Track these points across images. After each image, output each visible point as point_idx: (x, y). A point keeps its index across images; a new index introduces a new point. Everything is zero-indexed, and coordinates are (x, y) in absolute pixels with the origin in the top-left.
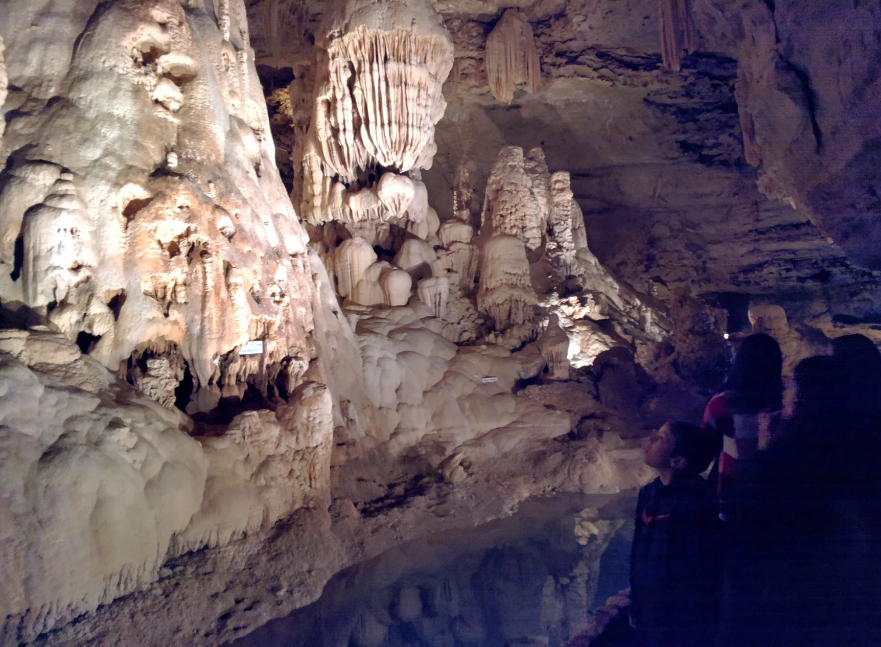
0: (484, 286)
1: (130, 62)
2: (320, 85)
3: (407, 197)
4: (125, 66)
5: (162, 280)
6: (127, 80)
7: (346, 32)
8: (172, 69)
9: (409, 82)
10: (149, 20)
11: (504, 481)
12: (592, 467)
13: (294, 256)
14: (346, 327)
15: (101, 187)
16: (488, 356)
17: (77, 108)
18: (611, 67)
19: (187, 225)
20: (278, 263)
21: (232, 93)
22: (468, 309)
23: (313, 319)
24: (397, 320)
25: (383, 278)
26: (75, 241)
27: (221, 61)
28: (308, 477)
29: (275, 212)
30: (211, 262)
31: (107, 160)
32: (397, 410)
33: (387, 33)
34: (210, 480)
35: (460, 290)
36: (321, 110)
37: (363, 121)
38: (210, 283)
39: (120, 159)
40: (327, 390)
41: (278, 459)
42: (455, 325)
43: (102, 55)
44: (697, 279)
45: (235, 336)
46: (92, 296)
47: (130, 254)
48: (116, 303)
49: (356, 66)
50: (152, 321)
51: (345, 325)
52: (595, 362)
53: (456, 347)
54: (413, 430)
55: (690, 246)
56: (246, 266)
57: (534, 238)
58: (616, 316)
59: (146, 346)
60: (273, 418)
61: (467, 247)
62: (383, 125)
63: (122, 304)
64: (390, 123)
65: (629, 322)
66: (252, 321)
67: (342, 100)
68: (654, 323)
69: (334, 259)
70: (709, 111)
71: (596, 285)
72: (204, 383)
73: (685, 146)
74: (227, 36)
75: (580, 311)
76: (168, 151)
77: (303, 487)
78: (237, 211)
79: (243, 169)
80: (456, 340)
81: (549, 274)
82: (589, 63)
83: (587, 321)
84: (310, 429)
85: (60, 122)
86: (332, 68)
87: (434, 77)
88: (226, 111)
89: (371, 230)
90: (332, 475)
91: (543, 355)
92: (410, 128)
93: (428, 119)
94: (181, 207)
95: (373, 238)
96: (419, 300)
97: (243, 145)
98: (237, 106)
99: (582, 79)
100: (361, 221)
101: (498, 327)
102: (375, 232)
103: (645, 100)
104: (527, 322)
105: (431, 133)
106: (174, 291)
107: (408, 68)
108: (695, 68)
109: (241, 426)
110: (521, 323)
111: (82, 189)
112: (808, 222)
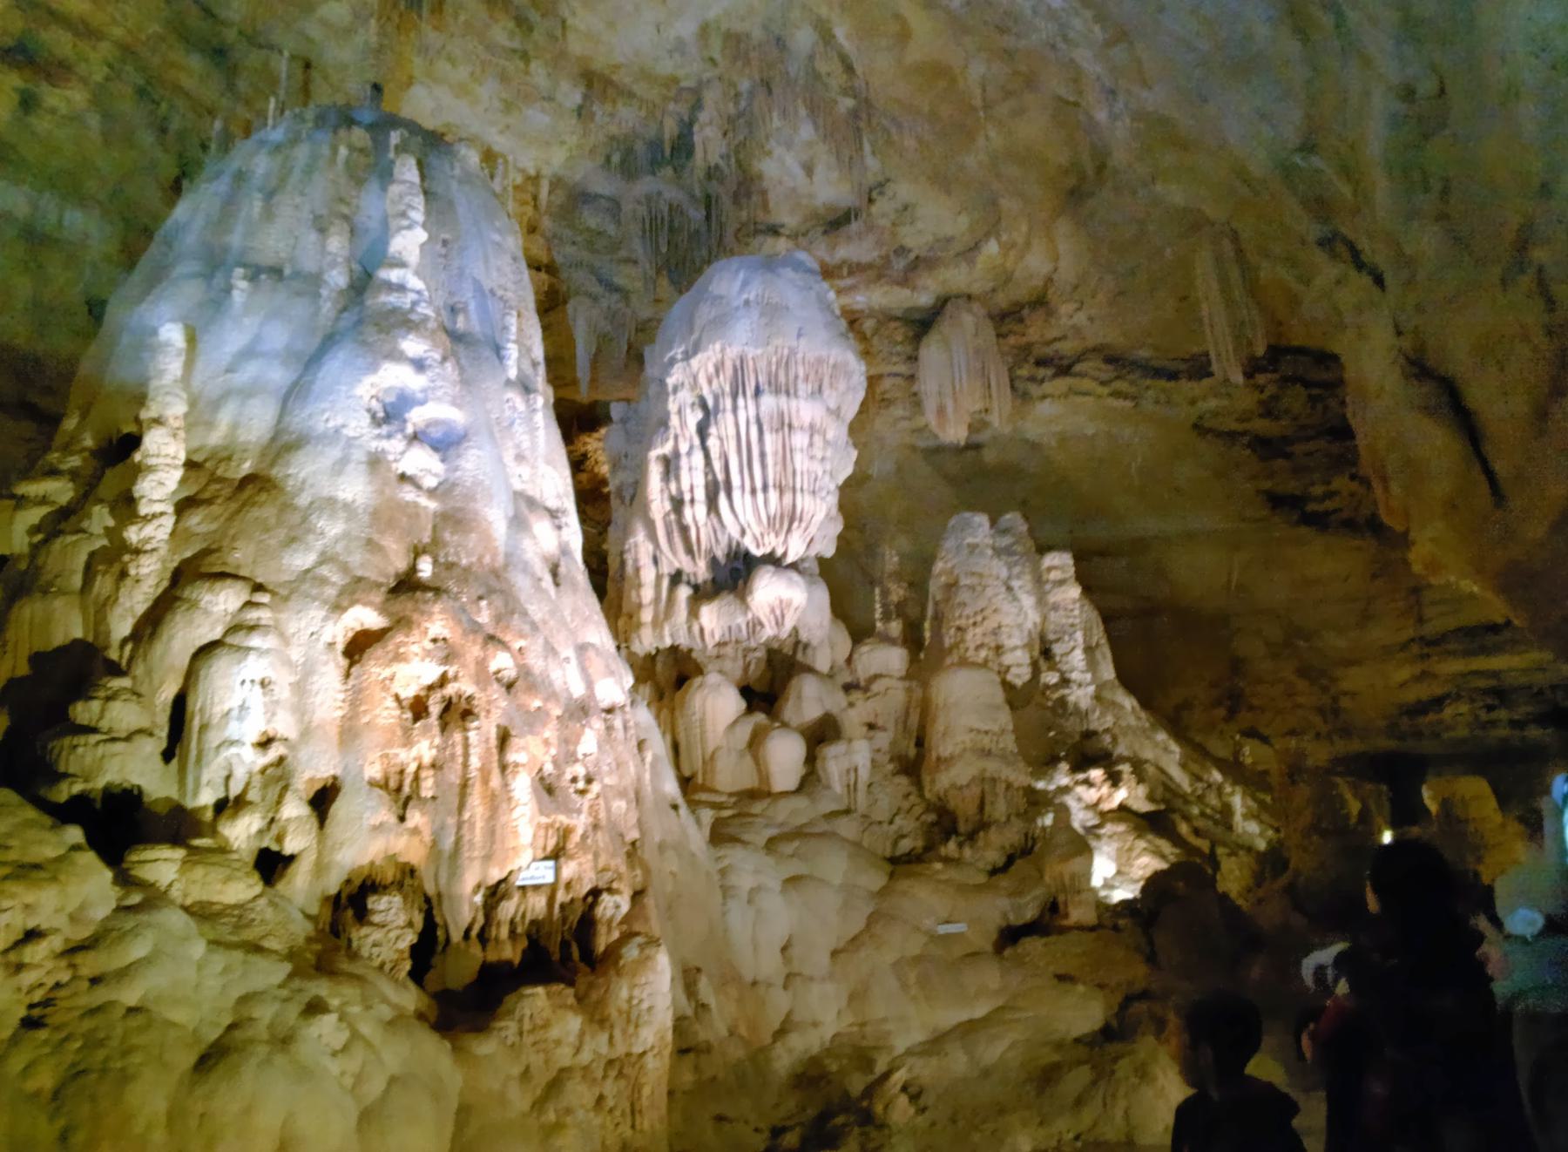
0: (934, 755)
1: (367, 419)
2: (655, 432)
3: (795, 603)
4: (358, 425)
5: (398, 761)
6: (361, 446)
7: (695, 353)
8: (428, 426)
9: (795, 423)
10: (397, 356)
11: (984, 1122)
12: (1147, 1092)
13: (610, 711)
14: (693, 831)
15: (312, 613)
16: (946, 882)
17: (282, 490)
18: (1131, 377)
19: (442, 669)
20: (583, 726)
21: (520, 458)
22: (907, 796)
23: (639, 821)
24: (780, 818)
25: (756, 742)
26: (267, 699)
27: (503, 411)
28: (628, 1111)
29: (580, 641)
30: (478, 728)
31: (325, 571)
32: (785, 987)
33: (759, 351)
34: (464, 1113)
35: (891, 760)
36: (655, 472)
37: (722, 486)
38: (475, 762)
39: (345, 568)
40: (663, 948)
41: (578, 1075)
42: (885, 826)
43: (324, 411)
44: (1324, 729)
45: (511, 853)
46: (285, 788)
47: (350, 719)
48: (323, 800)
49: (710, 403)
50: (378, 828)
51: (692, 830)
52: (1144, 890)
53: (888, 867)
54: (815, 1024)
55: (1303, 672)
56: (532, 732)
57: (1019, 665)
58: (1179, 803)
59: (366, 872)
60: (571, 1000)
61: (900, 685)
62: (753, 491)
63: (333, 800)
64: (765, 488)
65: (1203, 814)
66: (539, 826)
67: (689, 454)
68: (1248, 816)
69: (672, 711)
70: (1309, 439)
71: (1137, 747)
72: (456, 936)
73: (1277, 501)
74: (513, 373)
75: (1110, 795)
76: (417, 552)
77: (620, 1130)
78: (521, 643)
79: (533, 575)
80: (888, 854)
81: (1049, 729)
82: (1092, 373)
83: (1124, 814)
84: (633, 1020)
85: (255, 513)
86: (672, 407)
87: (836, 413)
88: (508, 485)
89: (735, 659)
90: (670, 1110)
91: (1047, 878)
92: (799, 495)
93: (827, 478)
94: (434, 641)
95: (738, 673)
96: (819, 780)
97: (534, 537)
98: (526, 477)
99: (1086, 399)
100: (720, 645)
101: (962, 827)
102: (740, 663)
103: (1195, 426)
104: (1013, 818)
105: (833, 500)
106: (416, 778)
107: (794, 403)
108: (1275, 371)
109: (517, 1014)
110: (1003, 819)
111: (283, 616)
112: (1508, 623)
